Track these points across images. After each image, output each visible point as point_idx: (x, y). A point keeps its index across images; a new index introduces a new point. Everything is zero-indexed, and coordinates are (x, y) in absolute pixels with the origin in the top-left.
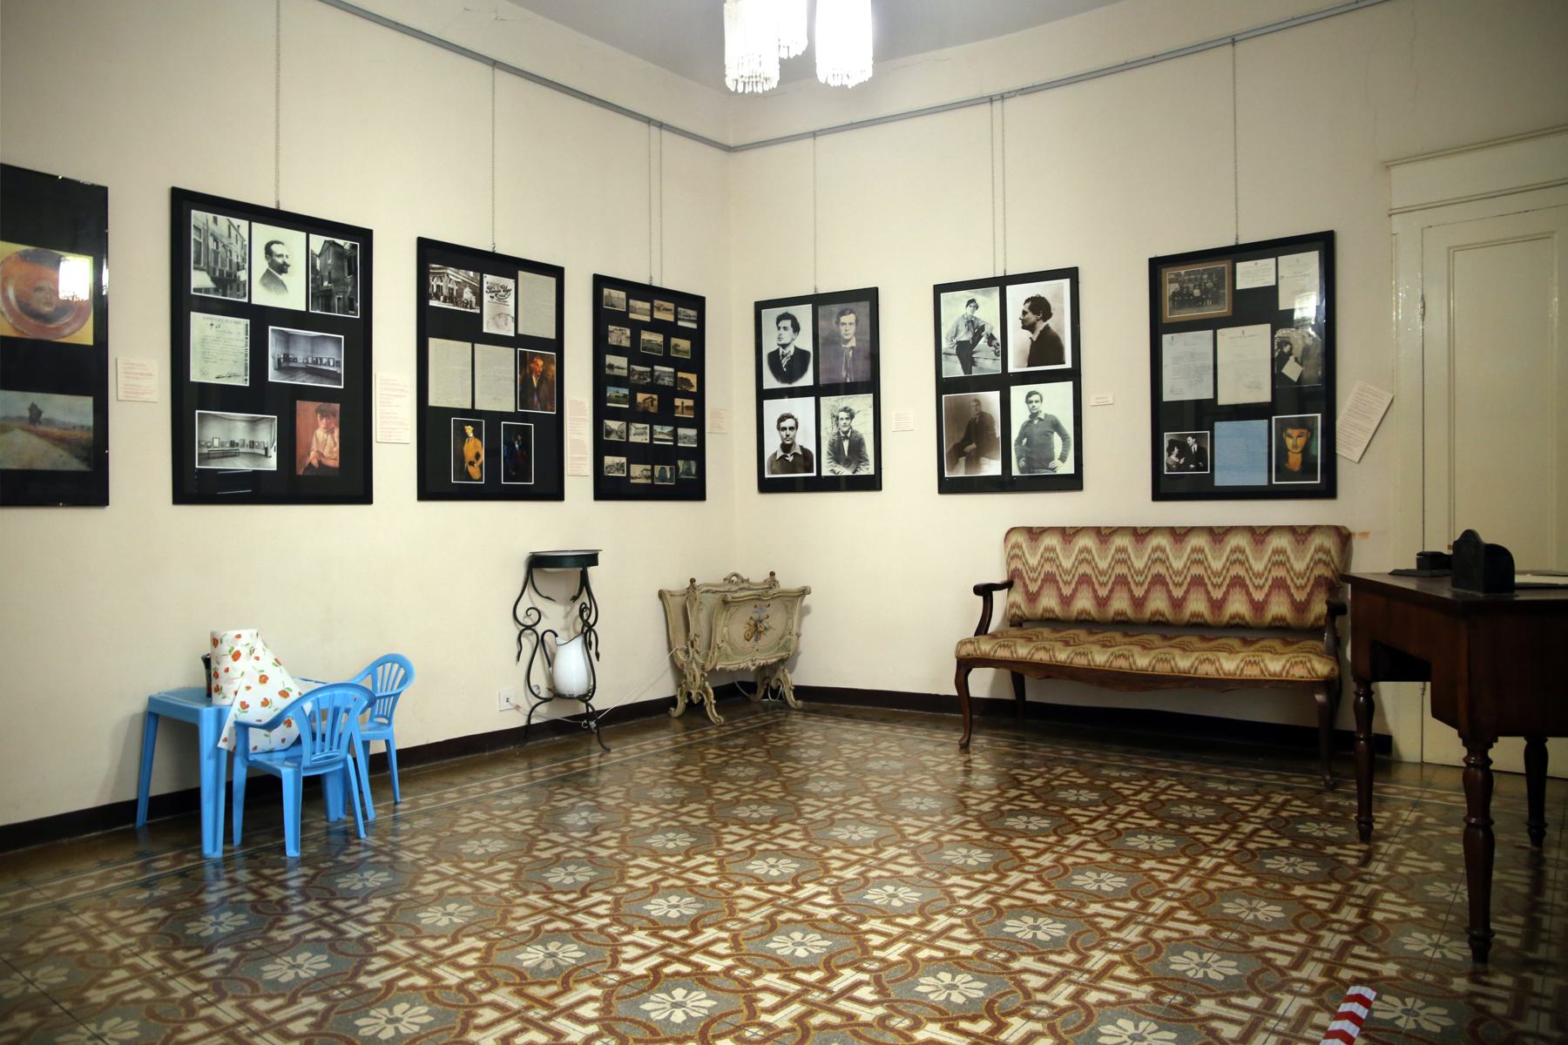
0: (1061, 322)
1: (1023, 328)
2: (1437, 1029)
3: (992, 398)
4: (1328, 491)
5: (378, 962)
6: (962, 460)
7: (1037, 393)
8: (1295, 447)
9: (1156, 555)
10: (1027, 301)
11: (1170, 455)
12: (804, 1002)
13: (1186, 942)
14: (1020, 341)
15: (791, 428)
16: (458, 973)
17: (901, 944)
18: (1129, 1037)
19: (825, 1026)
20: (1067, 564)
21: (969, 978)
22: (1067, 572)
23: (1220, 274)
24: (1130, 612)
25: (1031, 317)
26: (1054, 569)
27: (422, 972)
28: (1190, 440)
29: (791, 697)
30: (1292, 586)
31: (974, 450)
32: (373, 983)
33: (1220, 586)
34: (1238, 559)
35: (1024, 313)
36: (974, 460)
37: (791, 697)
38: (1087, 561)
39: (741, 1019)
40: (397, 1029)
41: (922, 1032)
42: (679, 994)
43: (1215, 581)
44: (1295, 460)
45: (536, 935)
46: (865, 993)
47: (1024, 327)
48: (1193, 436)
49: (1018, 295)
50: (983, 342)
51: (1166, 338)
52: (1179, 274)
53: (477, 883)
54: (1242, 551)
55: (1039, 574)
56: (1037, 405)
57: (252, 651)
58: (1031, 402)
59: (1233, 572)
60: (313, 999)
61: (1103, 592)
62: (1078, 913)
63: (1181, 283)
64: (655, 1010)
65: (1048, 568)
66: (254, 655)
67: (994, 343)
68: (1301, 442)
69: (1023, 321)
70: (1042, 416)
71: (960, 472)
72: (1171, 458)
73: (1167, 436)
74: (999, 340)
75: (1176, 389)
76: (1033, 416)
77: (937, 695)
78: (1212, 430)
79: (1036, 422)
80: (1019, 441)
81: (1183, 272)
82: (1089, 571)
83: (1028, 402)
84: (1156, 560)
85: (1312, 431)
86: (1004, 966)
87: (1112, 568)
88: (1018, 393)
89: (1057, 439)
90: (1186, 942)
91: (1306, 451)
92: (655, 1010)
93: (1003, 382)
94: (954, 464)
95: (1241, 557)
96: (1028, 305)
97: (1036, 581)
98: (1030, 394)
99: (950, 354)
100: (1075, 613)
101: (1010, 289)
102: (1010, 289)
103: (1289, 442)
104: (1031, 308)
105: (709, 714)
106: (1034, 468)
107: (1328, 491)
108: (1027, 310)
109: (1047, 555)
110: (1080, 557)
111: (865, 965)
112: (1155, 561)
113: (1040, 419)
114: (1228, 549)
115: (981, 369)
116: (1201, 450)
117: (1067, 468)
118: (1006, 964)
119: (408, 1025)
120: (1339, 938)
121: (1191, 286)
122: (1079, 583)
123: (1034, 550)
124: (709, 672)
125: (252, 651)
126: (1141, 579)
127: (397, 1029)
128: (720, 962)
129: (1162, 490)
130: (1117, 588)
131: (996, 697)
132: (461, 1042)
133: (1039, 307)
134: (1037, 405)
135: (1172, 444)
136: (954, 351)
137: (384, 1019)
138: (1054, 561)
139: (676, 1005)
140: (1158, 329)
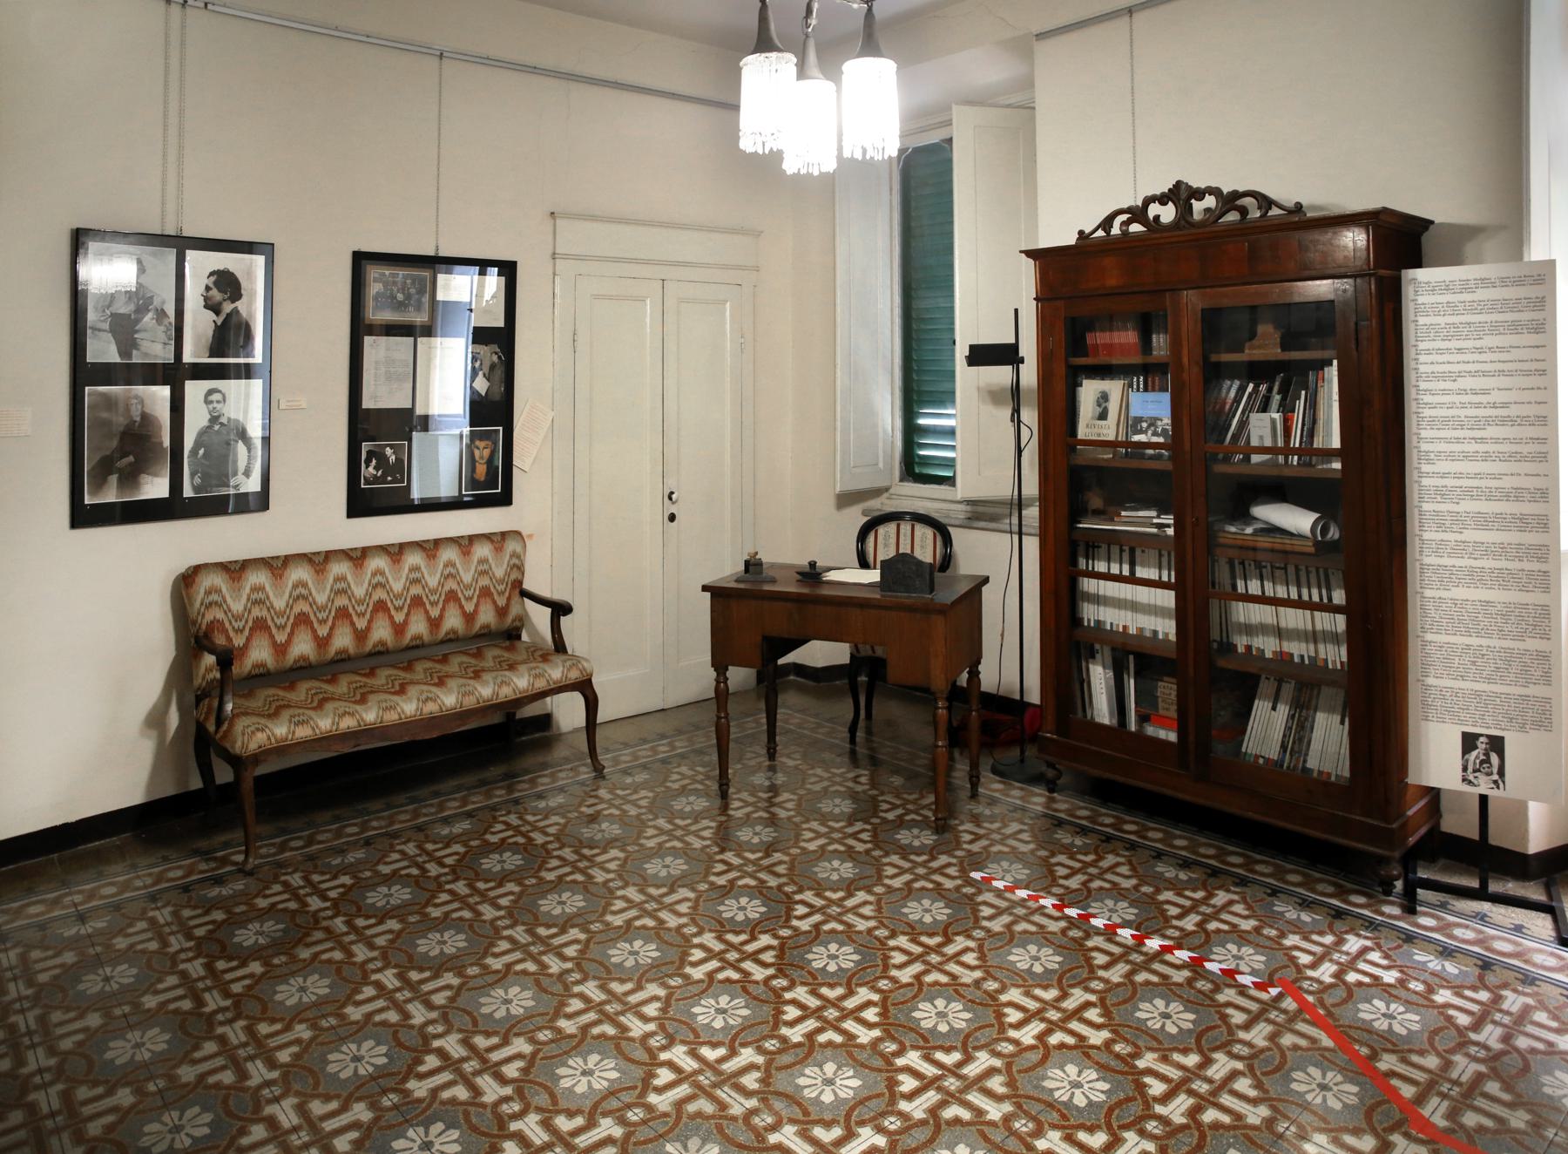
0: (254, 308)
1: (205, 307)
3: (161, 394)
4: (505, 499)
6: (113, 479)
7: (219, 391)
8: (482, 458)
9: (298, 591)
10: (212, 274)
11: (367, 467)
14: (199, 325)
15: (218, 402)
17: (812, 1021)
19: (1062, 1046)
20: (237, 606)
21: (1051, 952)
22: (280, 614)
23: (422, 280)
24: (427, 638)
25: (216, 295)
26: (265, 613)
28: (389, 451)
30: (314, 620)
31: (130, 464)
33: (436, 603)
34: (301, 593)
35: (208, 288)
36: (130, 478)
38: (303, 597)
43: (236, 625)
44: (481, 470)
46: (1093, 1014)
47: (206, 307)
48: (391, 446)
49: (200, 265)
50: (148, 318)
51: (368, 340)
52: (384, 275)
54: (305, 585)
55: (247, 622)
56: (219, 406)
58: (212, 402)
59: (297, 610)
61: (435, 613)
63: (386, 284)
65: (257, 612)
67: (166, 322)
68: (486, 453)
69: (206, 299)
70: (224, 420)
71: (110, 495)
72: (369, 471)
73: (365, 447)
74: (172, 318)
75: (377, 396)
76: (214, 419)
77: (66, 826)
78: (410, 440)
79: (217, 427)
80: (194, 452)
81: (387, 273)
82: (384, 596)
83: (207, 402)
84: (298, 597)
85: (495, 443)
86: (1152, 898)
87: (508, 574)
88: (194, 390)
89: (241, 448)
91: (490, 462)
93: (174, 374)
94: (99, 483)
95: (304, 591)
96: (213, 279)
97: (242, 631)
98: (211, 392)
99: (100, 330)
100: (291, 662)
101: (191, 255)
102: (191, 255)
103: (477, 453)
104: (215, 283)
106: (211, 486)
107: (505, 499)
108: (211, 285)
109: (254, 596)
110: (295, 594)
112: (375, 587)
113: (222, 424)
114: (290, 585)
115: (146, 355)
116: (399, 461)
117: (253, 485)
120: (32, 1066)
121: (395, 289)
122: (446, 601)
123: (320, 583)
126: (241, 624)
129: (361, 503)
130: (482, 600)
131: (157, 797)
133: (227, 284)
134: (219, 406)
135: (370, 454)
136: (106, 326)
138: (346, 592)
140: (360, 329)
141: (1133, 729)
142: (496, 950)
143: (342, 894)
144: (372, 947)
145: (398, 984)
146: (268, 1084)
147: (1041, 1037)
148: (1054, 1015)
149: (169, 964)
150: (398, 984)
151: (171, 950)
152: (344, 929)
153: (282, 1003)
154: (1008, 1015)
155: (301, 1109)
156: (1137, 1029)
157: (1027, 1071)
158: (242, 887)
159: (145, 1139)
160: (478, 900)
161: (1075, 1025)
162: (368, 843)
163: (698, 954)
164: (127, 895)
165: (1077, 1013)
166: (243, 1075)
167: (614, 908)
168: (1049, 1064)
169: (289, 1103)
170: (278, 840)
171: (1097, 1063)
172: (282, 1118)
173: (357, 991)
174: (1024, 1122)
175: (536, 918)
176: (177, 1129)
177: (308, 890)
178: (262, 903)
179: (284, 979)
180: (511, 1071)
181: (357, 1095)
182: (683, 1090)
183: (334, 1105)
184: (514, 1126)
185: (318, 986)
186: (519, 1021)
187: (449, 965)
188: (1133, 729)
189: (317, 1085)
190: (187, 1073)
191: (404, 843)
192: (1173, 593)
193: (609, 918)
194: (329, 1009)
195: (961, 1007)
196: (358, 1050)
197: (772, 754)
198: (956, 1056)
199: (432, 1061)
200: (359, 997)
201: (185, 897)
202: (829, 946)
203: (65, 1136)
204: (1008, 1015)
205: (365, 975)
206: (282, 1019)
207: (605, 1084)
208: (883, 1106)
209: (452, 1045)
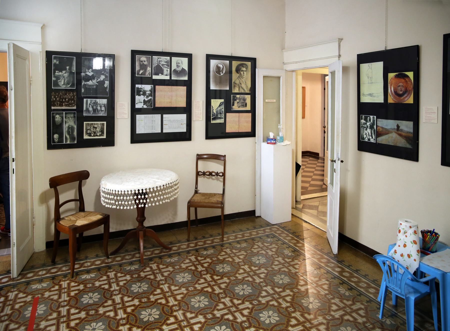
5: (223, 253)
12: (344, 311)
16: (238, 259)
19: (348, 320)
27: (232, 258)
32: (221, 258)
39: (294, 286)
42: (283, 276)
46: (362, 312)
53: (267, 251)
57: (405, 232)
60: (209, 259)
64: (305, 303)
66: (406, 234)
92: (305, 303)
119: (246, 292)
125: (405, 232)
128: (279, 260)
132: (286, 330)
137: (241, 288)
139: (281, 279)
141: (75, 271)
142: (221, 254)
145: (195, 260)
146: (161, 280)
147: (342, 316)
148: (348, 310)
150: (195, 260)
154: (333, 307)
159: (132, 288)
161: (354, 315)
162: (214, 247)
163: (241, 271)
165: (356, 311)
166: (156, 277)
169: (166, 285)
176: (140, 287)
180: (223, 286)
181: (183, 286)
182: (241, 307)
186: (226, 273)
188: (75, 271)
189: (127, 293)
190: (142, 274)
192: (160, 132)
195: (341, 292)
196: (184, 275)
199: (158, 291)
202: (282, 276)
203: (66, 294)
204: (333, 307)
207: (248, 293)
209: (165, 287)
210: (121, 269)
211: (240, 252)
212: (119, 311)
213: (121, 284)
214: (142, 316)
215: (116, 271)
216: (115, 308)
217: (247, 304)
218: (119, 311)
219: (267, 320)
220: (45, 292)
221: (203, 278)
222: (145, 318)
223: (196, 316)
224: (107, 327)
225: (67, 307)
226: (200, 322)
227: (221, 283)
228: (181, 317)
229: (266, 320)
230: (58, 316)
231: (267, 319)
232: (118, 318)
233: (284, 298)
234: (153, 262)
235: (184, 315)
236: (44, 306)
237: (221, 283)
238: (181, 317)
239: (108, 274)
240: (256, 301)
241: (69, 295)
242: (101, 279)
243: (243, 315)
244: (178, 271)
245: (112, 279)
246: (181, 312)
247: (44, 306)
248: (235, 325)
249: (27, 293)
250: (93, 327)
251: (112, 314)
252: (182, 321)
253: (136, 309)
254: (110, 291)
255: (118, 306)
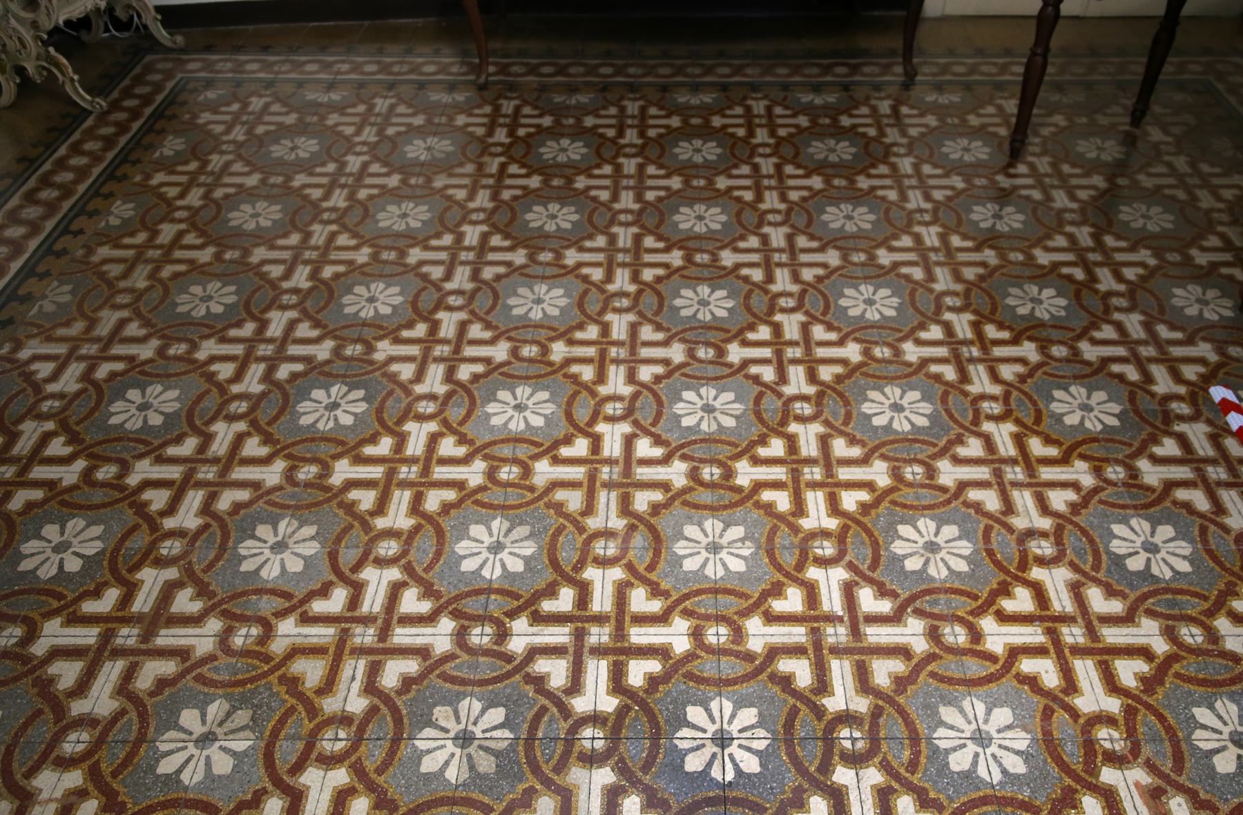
2: (681, 144)
13: (307, 167)
18: (326, 408)
29: (161, 34)
37: (161, 34)
40: (1204, 294)
41: (133, 475)
45: (1208, 274)
62: (287, 189)
90: (307, 167)
105: (78, 101)
111: (57, 404)
118: (165, 341)
124: (50, 33)
127: (1204, 294)
143: (923, 135)
144: (928, 198)
149: (748, 152)
151: (754, 141)
152: (909, 171)
153: (826, 224)
155: (805, 328)
156: (1169, 729)
157: (941, 679)
158: (710, 100)
160: (1056, 183)
162: (968, 87)
164: (737, 79)
167: (1205, 243)
168: (981, 690)
170: (1001, 61)
171: (1047, 734)
172: (786, 329)
173: (895, 237)
174: (857, 734)
175: (1110, 223)
177: (892, 121)
178: (974, 121)
179: (835, 201)
182: (1113, 636)
183: (833, 336)
184: (794, 428)
185: (864, 219)
187: (839, 243)
191: (1006, 98)
193: (1194, 252)
194: (864, 244)
197: (1138, 115)
198: (112, 595)
200: (896, 244)
201: (781, 95)
205: (910, 223)
206: (820, 239)
208: (732, 610)
210: (662, 98)
211: (1190, 341)
212: (612, 369)
213: (650, 196)
214: (681, 405)
215: (647, 101)
216: (603, 354)
217: (1148, 632)
218: (612, 369)
219: (1226, 753)
220: (412, 246)
221: (979, 435)
222: (691, 555)
223: (864, 461)
224: (518, 744)
225: (503, 159)
226: (869, 485)
227: (1053, 485)
228: (809, 447)
229: (1130, 555)
230: (348, 610)
231: (1137, 553)
232: (611, 288)
233: (1176, 364)
234: (759, 95)
235: (824, 441)
236: (363, 400)
237: (1053, 485)
238: (809, 447)
239: (625, 103)
240: (1195, 631)
241: (511, 134)
242: (588, 244)
243: (1044, 508)
244: (859, 272)
245: (629, 177)
246: (839, 574)
247: (363, 400)
248: (965, 417)
249: (362, 237)
250: (464, 720)
251: (597, 274)
252: (810, 461)
253: (669, 375)
254: (610, 209)
255: (613, 352)
